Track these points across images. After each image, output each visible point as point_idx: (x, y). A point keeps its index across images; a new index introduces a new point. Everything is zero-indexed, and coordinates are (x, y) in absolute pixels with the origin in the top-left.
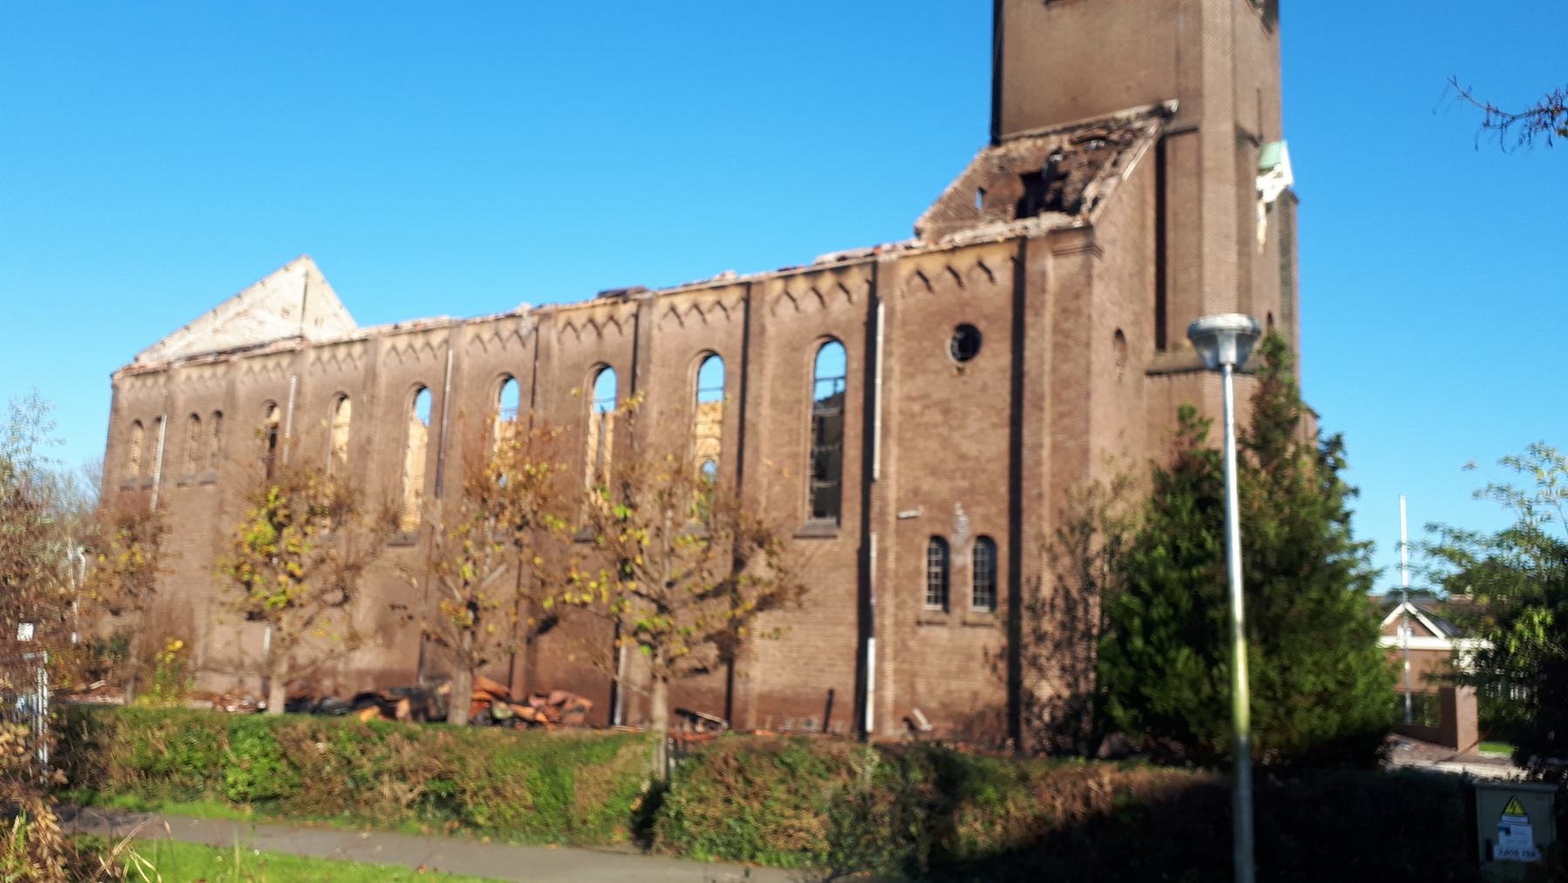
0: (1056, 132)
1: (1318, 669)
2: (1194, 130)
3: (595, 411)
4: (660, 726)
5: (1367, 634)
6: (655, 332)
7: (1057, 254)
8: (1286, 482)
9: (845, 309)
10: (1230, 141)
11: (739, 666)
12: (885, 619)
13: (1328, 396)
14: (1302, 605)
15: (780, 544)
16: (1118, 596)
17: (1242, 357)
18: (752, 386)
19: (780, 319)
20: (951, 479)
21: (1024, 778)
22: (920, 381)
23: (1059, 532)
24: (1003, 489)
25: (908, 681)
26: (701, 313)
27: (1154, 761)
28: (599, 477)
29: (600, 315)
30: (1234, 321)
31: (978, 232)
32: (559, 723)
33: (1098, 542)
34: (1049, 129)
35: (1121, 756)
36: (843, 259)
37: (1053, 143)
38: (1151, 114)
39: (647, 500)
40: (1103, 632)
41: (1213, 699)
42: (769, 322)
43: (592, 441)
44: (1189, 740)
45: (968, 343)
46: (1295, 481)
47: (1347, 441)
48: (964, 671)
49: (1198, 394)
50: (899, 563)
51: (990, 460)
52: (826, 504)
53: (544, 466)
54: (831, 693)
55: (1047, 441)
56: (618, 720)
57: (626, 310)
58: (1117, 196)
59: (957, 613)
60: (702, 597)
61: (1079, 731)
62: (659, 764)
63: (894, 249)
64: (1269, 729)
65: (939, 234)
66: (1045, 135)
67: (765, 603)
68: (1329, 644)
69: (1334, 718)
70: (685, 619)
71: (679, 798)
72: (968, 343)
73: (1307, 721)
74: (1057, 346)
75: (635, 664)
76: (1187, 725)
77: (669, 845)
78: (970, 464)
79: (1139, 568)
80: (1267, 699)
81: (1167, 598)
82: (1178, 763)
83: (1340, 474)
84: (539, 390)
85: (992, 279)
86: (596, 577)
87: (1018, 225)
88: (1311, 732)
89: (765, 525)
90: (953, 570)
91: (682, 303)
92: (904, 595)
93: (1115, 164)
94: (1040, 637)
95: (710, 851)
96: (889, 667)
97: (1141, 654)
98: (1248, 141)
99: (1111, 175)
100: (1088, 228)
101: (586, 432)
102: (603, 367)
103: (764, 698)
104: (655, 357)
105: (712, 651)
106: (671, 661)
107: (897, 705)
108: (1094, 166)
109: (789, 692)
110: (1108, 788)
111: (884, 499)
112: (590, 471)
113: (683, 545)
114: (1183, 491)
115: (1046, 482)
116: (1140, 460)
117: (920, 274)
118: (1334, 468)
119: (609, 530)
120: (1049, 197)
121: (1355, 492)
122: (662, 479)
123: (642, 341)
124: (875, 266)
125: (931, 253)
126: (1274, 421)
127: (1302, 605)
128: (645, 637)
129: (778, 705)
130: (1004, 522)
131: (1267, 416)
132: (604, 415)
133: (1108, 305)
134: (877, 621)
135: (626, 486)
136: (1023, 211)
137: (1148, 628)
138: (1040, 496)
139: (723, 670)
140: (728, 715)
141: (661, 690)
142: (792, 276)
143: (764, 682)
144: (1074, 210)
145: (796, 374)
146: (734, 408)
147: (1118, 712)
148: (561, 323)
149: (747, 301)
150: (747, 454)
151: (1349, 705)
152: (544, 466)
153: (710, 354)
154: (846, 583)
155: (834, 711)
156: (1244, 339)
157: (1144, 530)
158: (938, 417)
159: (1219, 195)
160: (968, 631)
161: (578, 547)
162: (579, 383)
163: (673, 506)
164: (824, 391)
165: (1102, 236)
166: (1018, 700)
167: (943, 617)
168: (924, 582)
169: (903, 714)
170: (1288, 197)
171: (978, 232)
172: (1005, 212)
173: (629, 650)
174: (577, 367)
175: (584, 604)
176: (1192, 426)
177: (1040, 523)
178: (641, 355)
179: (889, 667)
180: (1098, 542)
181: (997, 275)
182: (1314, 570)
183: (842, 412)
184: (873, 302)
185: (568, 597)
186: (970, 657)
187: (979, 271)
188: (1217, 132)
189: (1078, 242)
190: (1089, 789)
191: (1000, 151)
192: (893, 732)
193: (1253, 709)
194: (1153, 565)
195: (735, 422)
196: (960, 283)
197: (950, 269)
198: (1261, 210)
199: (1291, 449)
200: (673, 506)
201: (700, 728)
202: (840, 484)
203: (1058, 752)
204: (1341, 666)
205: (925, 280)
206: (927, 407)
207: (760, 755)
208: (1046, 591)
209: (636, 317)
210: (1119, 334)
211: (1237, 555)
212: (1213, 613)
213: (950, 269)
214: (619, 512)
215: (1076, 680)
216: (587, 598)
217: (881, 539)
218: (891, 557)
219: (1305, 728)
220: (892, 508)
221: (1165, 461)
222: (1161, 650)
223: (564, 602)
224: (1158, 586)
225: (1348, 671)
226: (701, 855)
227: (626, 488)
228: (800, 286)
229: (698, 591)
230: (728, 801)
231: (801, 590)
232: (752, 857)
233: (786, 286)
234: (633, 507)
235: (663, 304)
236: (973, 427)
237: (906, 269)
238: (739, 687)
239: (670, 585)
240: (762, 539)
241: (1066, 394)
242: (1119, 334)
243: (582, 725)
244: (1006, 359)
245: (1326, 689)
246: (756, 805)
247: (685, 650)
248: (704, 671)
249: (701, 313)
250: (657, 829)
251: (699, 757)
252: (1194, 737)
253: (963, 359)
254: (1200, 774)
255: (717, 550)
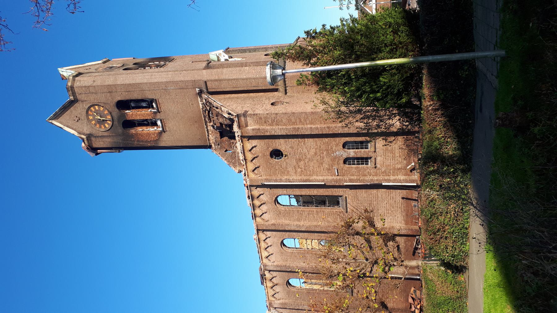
0: (207, 128)
1: (385, 35)
2: (206, 82)
3: (304, 286)
4: (420, 263)
5: (373, 19)
6: (275, 264)
7: (247, 126)
8: (321, 49)
9: (266, 196)
10: (209, 71)
11: (396, 232)
12: (375, 179)
13: (290, 34)
14: (363, 41)
15: (350, 218)
16: (362, 102)
17: (280, 67)
18: (293, 228)
19: (270, 219)
20: (323, 158)
21: (430, 132)
22: (290, 169)
23: (340, 122)
24: (326, 140)
25: (397, 171)
26: (268, 247)
27: (421, 88)
28: (327, 285)
29: (269, 284)
30: (268, 69)
31: (240, 152)
32: (420, 300)
33: (343, 108)
34: (206, 130)
35: (420, 98)
36: (249, 197)
37: (211, 128)
38: (201, 97)
39: (336, 268)
40: (375, 106)
41: (397, 69)
42: (270, 223)
43: (315, 287)
44: (412, 75)
45: (277, 154)
46: (321, 46)
47: (306, 30)
48: (392, 152)
49: (292, 77)
50: (355, 174)
51: (317, 145)
52: (334, 201)
53: (325, 307)
54: (403, 198)
55: (309, 126)
56: (418, 278)
57: (268, 275)
58: (228, 106)
59: (371, 154)
60: (371, 247)
61: (411, 112)
62: (434, 264)
63: (245, 180)
64: (407, 49)
65: (240, 164)
66: (208, 130)
67: (372, 224)
68: (376, 31)
69: (402, 28)
70: (380, 254)
71: (447, 257)
72: (277, 154)
73: (403, 37)
74: (277, 125)
75: (397, 271)
76: (407, 77)
77: (464, 260)
78: (318, 150)
79: (352, 96)
80: (397, 50)
81: (362, 86)
82: (421, 79)
83: (318, 31)
84: (297, 308)
85: (255, 147)
86: (365, 288)
87: (237, 138)
88: (407, 35)
89: (343, 224)
90: (355, 156)
91: (265, 254)
92: (366, 173)
93: (217, 108)
94: (378, 126)
95: (465, 244)
96: (392, 178)
97: (383, 94)
98: (209, 65)
99: (221, 109)
100: (238, 116)
101: (312, 289)
102: (288, 283)
103: (407, 223)
104: (284, 264)
105: (391, 243)
106: (395, 259)
107: (406, 175)
108: (218, 115)
109: (404, 214)
110: (432, 102)
111: (331, 181)
112: (326, 288)
113: (352, 256)
114: (325, 82)
115: (323, 126)
116: (314, 96)
117: (253, 171)
118: (316, 33)
119: (348, 282)
120: (228, 129)
121: (324, 26)
122: (328, 263)
123: (279, 269)
124: (251, 186)
125: (246, 167)
126: (301, 54)
127: (363, 41)
128: (387, 268)
129: (409, 217)
130: (337, 139)
131: (299, 56)
132: (305, 282)
133: (263, 108)
134: (376, 182)
135: (331, 276)
136: (234, 138)
137: (373, 92)
138: (328, 127)
139: (398, 238)
140: (415, 236)
141: (406, 263)
142: (255, 214)
143: (401, 222)
144: (232, 121)
145: (288, 211)
146: (301, 234)
147: (404, 100)
148: (273, 299)
149: (263, 231)
150: (317, 230)
151: (397, 24)
152: (325, 307)
153: (282, 244)
154: (362, 193)
155: (410, 197)
156: (274, 67)
157: (339, 94)
158: (302, 162)
159: (227, 74)
160: (377, 150)
161: (355, 295)
162: (294, 292)
163: (338, 259)
164: (294, 202)
165: (240, 111)
166: (401, 133)
167: (373, 159)
168: (360, 166)
169: (409, 172)
170: (227, 51)
171: (240, 152)
172: (233, 143)
173: (391, 274)
174: (288, 293)
175: (376, 292)
176: (303, 80)
177: (338, 127)
178: (284, 269)
179: (392, 178)
180: (343, 108)
181: (253, 145)
182: (351, 38)
183: (301, 196)
184: (263, 186)
185: (373, 298)
186: (387, 149)
187: (252, 151)
188: (206, 75)
189: (242, 119)
190: (433, 109)
191: (213, 145)
192: (416, 176)
193: (400, 57)
194: (351, 91)
195: (306, 234)
196: (256, 157)
197: (252, 161)
198: (230, 60)
199: (310, 48)
200: (338, 259)
201: (420, 246)
202: (327, 196)
203: (420, 120)
204: (384, 27)
205: (256, 168)
206: (299, 166)
207: (428, 226)
208: (362, 125)
209: (270, 271)
210: (272, 104)
211: (346, 63)
212: (367, 70)
213: (252, 161)
214: (341, 277)
215: (393, 114)
216: (373, 291)
217: (346, 181)
218: (352, 177)
219: (406, 38)
220: (335, 178)
221: (315, 88)
222: (381, 87)
223: (375, 299)
224: (358, 89)
225: (385, 24)
226: (467, 248)
227: (331, 276)
228: (258, 212)
229: (369, 249)
230: (446, 238)
231: (366, 211)
232: (467, 229)
233: (258, 217)
234: (339, 274)
235: (265, 261)
236: (305, 150)
237: (252, 175)
238: (403, 232)
239: (367, 260)
240: (348, 225)
241: (293, 120)
242: (272, 104)
243: (421, 291)
244: (282, 141)
245: (392, 31)
246: (447, 228)
247: (391, 254)
248: (398, 246)
249: (268, 247)
250: (458, 264)
251: (430, 249)
252: (411, 74)
253: (282, 155)
254: (425, 71)
255: (353, 242)
